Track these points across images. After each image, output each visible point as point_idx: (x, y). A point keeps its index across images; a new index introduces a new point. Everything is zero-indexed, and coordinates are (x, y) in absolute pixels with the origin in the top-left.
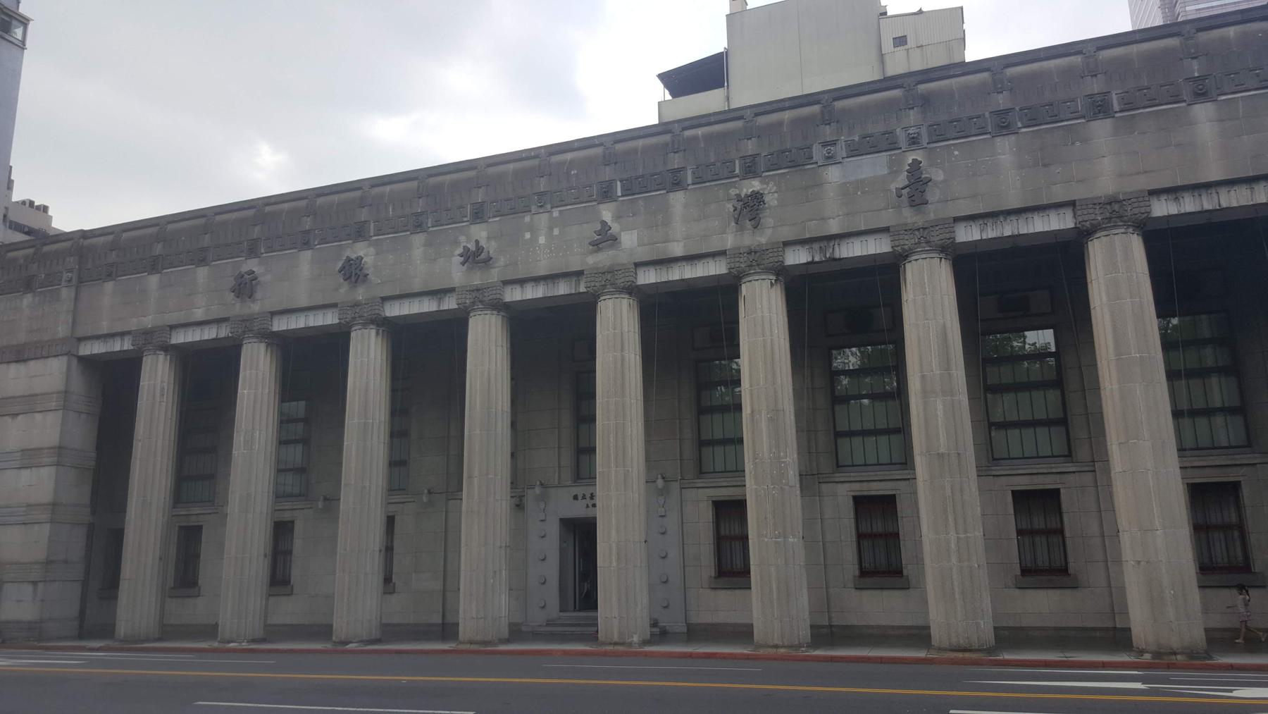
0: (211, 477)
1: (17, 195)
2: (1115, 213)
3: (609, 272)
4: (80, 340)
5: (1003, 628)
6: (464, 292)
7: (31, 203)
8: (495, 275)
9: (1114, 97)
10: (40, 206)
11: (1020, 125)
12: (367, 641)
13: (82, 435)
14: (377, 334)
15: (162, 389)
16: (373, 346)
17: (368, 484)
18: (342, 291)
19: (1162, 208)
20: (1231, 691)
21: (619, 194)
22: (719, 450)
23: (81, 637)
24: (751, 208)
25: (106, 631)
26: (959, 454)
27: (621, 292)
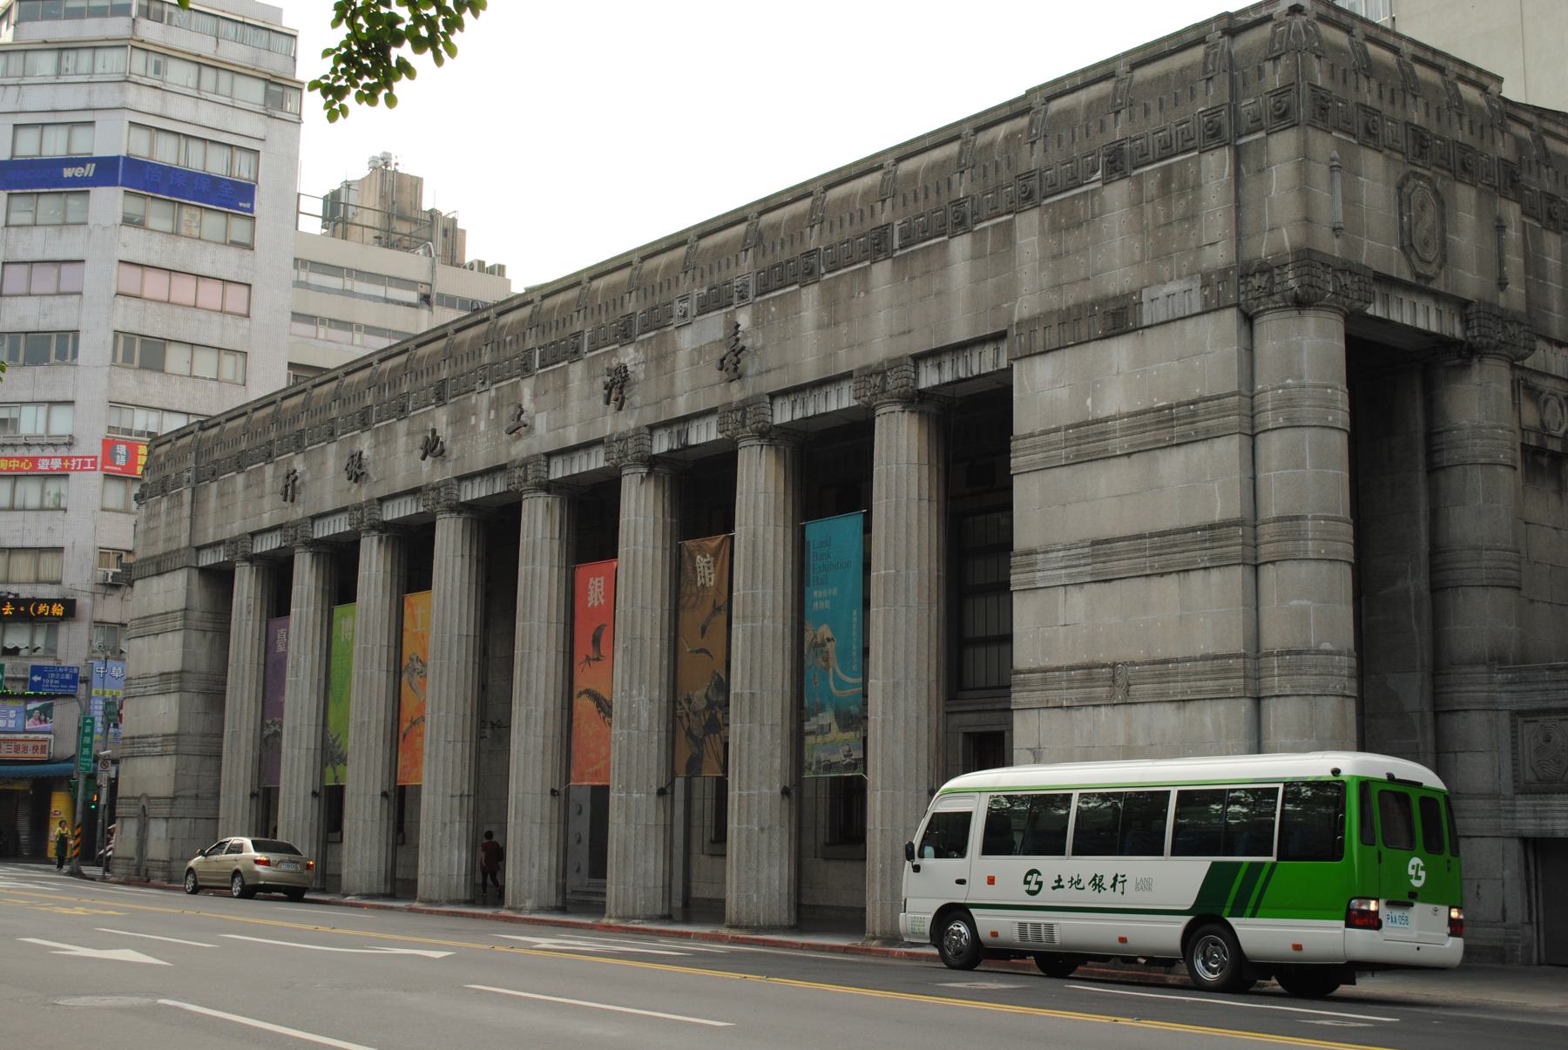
2: (1261, 290)
3: (877, 374)
4: (199, 549)
6: (863, 378)
7: (481, 264)
8: (448, 471)
9: (896, 229)
10: (494, 266)
12: (366, 895)
14: (380, 541)
15: (249, 606)
19: (929, 378)
21: (537, 366)
22: (981, 651)
23: (562, 910)
25: (713, 911)
27: (536, 491)
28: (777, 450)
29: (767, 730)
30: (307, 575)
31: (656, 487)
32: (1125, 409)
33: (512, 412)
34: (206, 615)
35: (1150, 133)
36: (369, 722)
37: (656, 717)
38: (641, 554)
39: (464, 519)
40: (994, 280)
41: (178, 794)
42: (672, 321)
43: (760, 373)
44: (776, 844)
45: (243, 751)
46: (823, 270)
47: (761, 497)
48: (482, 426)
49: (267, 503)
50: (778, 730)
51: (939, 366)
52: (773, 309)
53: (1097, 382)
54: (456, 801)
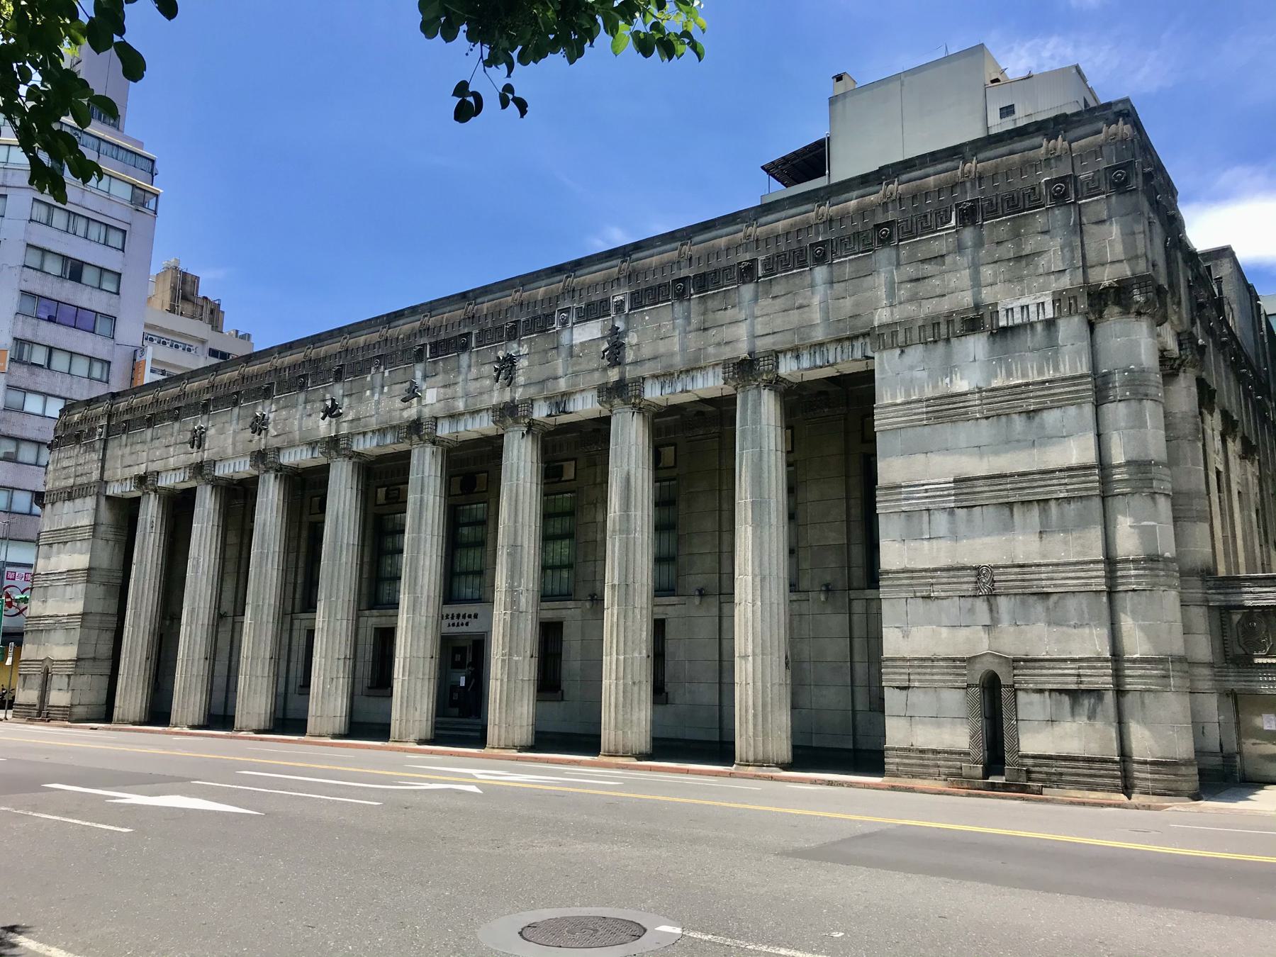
0: (480, 573)
1: (201, 294)
5: (543, 733)
11: (692, 291)
13: (107, 557)
14: (276, 477)
16: (427, 462)
17: (261, 603)
18: (496, 394)
20: (627, 786)
21: (428, 356)
24: (507, 367)
26: (627, 585)
28: (644, 416)
29: (637, 611)
30: (207, 501)
31: (533, 440)
34: (109, 529)
36: (263, 606)
37: (531, 602)
38: (522, 486)
39: (354, 463)
41: (81, 657)
43: (635, 363)
44: (643, 695)
45: (142, 625)
46: (692, 291)
47: (633, 448)
50: (644, 612)
51: (798, 357)
52: (647, 318)
54: (341, 662)
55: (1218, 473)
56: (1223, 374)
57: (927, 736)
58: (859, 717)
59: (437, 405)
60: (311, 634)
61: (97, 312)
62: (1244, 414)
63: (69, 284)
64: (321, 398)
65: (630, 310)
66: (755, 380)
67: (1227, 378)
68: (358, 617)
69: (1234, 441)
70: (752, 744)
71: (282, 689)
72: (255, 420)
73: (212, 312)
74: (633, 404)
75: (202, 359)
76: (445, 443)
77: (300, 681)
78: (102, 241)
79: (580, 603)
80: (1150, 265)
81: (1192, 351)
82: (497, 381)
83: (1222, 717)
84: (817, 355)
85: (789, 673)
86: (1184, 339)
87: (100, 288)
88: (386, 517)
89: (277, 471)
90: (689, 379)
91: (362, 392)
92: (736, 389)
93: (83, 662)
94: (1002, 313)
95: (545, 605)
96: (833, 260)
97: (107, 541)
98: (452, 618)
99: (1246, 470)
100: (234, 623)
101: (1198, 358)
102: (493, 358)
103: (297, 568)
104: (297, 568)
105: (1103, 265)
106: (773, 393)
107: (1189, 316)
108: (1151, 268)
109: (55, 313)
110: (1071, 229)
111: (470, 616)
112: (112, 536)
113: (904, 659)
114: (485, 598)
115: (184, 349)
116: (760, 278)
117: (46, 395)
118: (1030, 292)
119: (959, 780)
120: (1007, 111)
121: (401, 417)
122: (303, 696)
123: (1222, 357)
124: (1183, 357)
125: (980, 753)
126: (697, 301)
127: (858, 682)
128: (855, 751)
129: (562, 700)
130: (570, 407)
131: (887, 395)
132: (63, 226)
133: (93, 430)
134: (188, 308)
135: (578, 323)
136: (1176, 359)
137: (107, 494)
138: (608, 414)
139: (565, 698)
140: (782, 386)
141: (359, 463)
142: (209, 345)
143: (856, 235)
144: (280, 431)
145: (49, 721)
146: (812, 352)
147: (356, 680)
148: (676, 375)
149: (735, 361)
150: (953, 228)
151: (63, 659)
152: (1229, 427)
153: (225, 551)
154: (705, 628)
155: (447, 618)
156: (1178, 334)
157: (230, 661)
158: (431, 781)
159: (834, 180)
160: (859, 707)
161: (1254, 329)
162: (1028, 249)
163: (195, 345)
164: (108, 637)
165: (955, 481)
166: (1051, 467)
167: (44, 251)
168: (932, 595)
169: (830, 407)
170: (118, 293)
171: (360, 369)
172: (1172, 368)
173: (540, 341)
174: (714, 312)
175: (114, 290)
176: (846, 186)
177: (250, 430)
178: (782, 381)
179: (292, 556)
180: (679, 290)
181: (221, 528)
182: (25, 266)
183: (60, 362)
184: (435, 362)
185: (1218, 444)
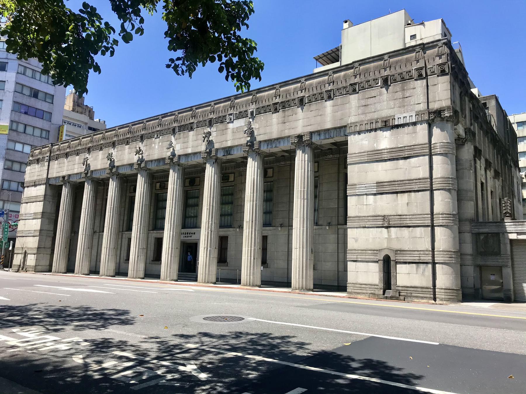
1: (85, 104)
13: (50, 209)
14: (117, 178)
31: (217, 165)
32: (388, 147)
33: (169, 143)
34: (50, 197)
35: (312, 95)
39: (147, 173)
40: (341, 112)
42: (226, 120)
48: (157, 147)
49: (76, 166)
51: (319, 135)
52: (262, 118)
53: (379, 139)
55: (482, 184)
56: (487, 145)
57: (362, 279)
58: (340, 273)
59: (180, 150)
60: (130, 240)
61: (44, 111)
62: (496, 162)
63: (33, 99)
64: (135, 147)
65: (256, 115)
66: (303, 143)
67: (489, 146)
68: (148, 233)
69: (490, 171)
70: (298, 281)
71: (118, 261)
72: (108, 155)
73: (90, 111)
74: (256, 152)
75: (85, 131)
76: (183, 166)
77: (125, 258)
78: (46, 82)
79: (235, 229)
80: (453, 102)
81: (470, 136)
82: (204, 142)
83: (475, 275)
84: (327, 134)
85: (313, 255)
86: (467, 131)
87: (45, 101)
88: (160, 195)
89: (117, 175)
90: (278, 142)
91: (151, 144)
92: (296, 147)
93: (40, 249)
94: (396, 119)
95: (221, 229)
96: (334, 97)
97: (50, 202)
98: (185, 234)
99: (495, 183)
100: (99, 235)
101: (472, 138)
102: (202, 133)
103: (124, 214)
104: (124, 214)
105: (435, 102)
106: (310, 148)
107: (470, 123)
108: (453, 103)
109: (28, 111)
110: (423, 88)
111: (192, 233)
112: (51, 200)
113: (355, 250)
114: (197, 226)
115: (78, 127)
116: (306, 103)
117: (24, 144)
118: (407, 112)
119: (374, 296)
120: (413, 37)
121: (166, 154)
122: (126, 264)
123: (486, 139)
124: (467, 138)
125: (381, 285)
126: (282, 112)
127: (340, 260)
128: (338, 286)
129: (227, 266)
130: (232, 152)
131: (351, 149)
132: (30, 75)
133: (44, 158)
134: (80, 109)
135: (236, 119)
136: (464, 138)
137: (50, 183)
138: (247, 155)
139: (229, 265)
140: (313, 146)
141: (149, 173)
142: (89, 125)
143: (343, 88)
144: (118, 160)
145: (26, 272)
146: (325, 133)
147: (147, 258)
148: (273, 141)
149: (296, 136)
150: (379, 86)
151: (32, 247)
152: (488, 165)
153: (96, 207)
154: (283, 240)
155: (183, 234)
156: (465, 129)
157: (98, 250)
158: (176, 288)
159: (343, 64)
160: (340, 270)
161: (504, 128)
162: (407, 95)
163: (83, 125)
164: (50, 240)
165: (377, 183)
166: (412, 178)
167: (23, 85)
168: (366, 226)
169: (333, 155)
170: (53, 103)
171: (150, 136)
172: (462, 142)
173: (220, 126)
174: (288, 116)
175: (51, 102)
176: (348, 67)
177: (107, 159)
178: (313, 144)
179: (123, 209)
180: (275, 108)
181: (94, 197)
182: (15, 91)
183: (29, 130)
184: (180, 134)
185: (483, 172)
